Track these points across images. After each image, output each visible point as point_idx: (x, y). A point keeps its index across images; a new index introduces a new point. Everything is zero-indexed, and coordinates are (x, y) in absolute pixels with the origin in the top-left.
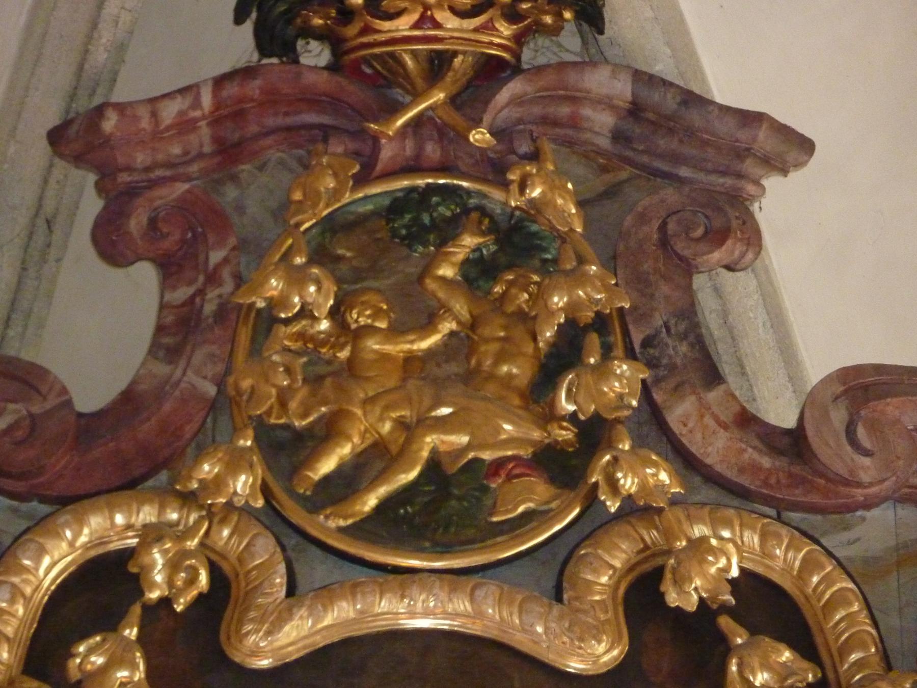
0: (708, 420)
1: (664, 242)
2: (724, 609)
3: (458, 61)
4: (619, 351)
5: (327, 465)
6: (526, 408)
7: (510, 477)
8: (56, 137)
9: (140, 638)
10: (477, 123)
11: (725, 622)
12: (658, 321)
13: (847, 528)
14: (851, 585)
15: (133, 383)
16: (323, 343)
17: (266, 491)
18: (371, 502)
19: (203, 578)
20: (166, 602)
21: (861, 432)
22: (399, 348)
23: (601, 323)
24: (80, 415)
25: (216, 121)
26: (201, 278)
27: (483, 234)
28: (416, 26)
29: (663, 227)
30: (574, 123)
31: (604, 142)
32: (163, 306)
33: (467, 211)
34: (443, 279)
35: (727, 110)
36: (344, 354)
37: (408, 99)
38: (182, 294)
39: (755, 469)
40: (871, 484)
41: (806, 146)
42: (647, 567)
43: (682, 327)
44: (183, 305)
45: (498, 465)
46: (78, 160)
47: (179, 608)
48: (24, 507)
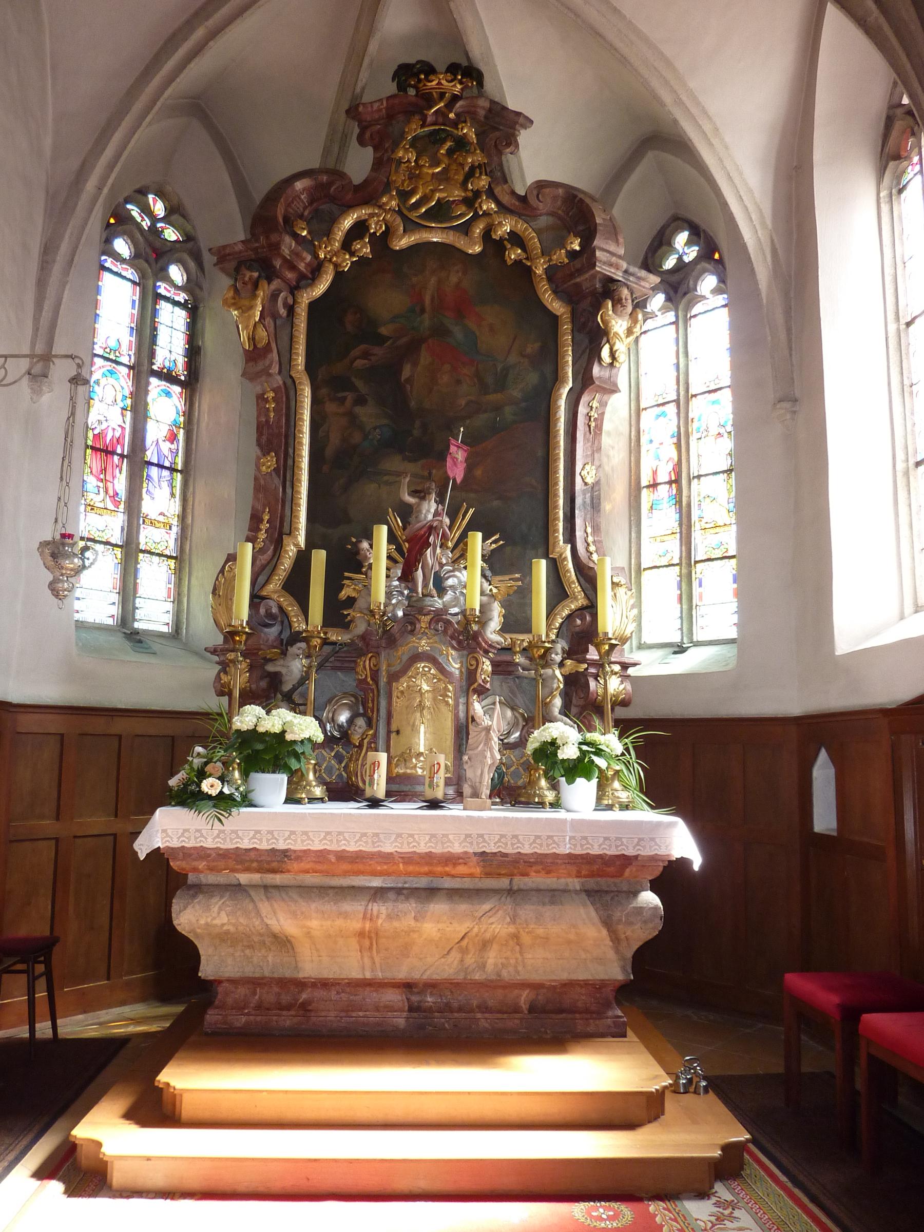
1: (496, 146)
2: (506, 239)
5: (413, 200)
7: (457, 205)
11: (506, 242)
18: (424, 210)
19: (384, 228)
20: (375, 233)
22: (430, 171)
23: (480, 166)
28: (437, 84)
29: (496, 142)
33: (448, 136)
36: (417, 172)
38: (378, 155)
41: (532, 122)
46: (353, 118)
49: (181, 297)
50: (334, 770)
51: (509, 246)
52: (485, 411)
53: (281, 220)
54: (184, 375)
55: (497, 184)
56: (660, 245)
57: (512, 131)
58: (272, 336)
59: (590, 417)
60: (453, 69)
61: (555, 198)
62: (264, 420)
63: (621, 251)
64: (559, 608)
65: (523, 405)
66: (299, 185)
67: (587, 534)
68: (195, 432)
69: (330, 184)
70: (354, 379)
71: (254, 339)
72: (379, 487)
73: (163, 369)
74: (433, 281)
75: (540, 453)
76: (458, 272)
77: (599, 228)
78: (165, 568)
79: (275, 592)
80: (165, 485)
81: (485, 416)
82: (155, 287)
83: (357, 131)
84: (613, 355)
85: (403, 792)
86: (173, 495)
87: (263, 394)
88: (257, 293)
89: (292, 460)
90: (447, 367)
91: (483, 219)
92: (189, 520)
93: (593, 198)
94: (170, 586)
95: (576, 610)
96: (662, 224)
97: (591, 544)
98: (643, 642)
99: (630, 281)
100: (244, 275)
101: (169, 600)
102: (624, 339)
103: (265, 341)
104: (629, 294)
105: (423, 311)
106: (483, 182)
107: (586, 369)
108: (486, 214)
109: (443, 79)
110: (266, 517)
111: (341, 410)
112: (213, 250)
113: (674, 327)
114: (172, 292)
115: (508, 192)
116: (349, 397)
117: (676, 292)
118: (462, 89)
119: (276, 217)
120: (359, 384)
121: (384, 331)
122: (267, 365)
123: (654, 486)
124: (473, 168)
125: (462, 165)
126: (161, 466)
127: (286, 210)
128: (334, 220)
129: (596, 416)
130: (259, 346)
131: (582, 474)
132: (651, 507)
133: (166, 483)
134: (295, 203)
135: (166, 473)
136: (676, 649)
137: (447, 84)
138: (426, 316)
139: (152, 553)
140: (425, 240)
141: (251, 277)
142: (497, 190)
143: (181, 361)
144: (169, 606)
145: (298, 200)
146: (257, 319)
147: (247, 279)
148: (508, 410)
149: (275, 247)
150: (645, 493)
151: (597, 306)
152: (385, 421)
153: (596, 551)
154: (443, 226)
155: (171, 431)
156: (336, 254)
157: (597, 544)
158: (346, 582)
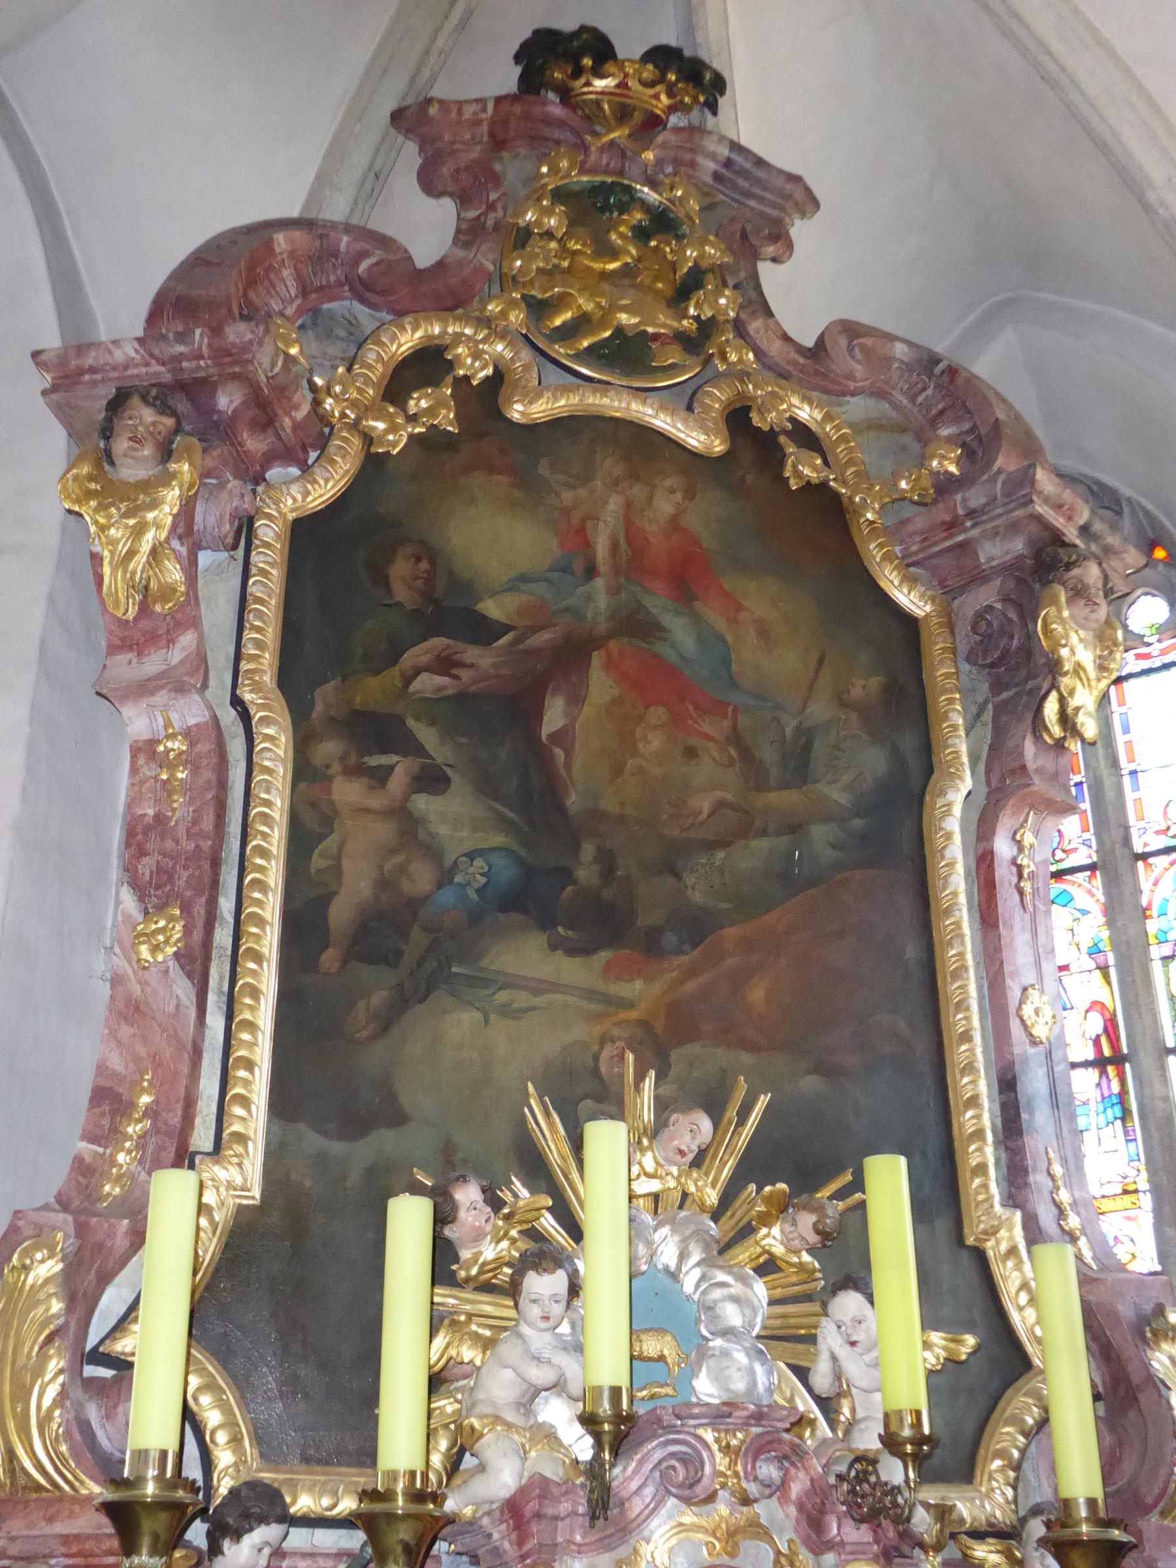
5: (558, 322)
7: (663, 344)
8: (397, 117)
9: (452, 395)
11: (782, 439)
13: (840, 405)
18: (585, 344)
20: (467, 378)
22: (597, 266)
25: (492, 123)
26: (484, 207)
29: (743, 229)
30: (692, 164)
35: (781, 172)
37: (603, 131)
38: (472, 214)
39: (795, 363)
40: (861, 380)
41: (816, 204)
42: (738, 405)
44: (473, 220)
45: (655, 337)
46: (408, 132)
47: (475, 383)
48: (378, 314)
52: (764, 832)
62: (151, 812)
65: (857, 823)
70: (411, 723)
72: (487, 1021)
74: (614, 503)
75: (912, 951)
76: (672, 491)
81: (762, 845)
90: (657, 714)
102: (1093, 683)
105: (591, 572)
109: (634, 76)
111: (376, 802)
112: (44, 357)
115: (779, 333)
116: (399, 769)
120: (427, 736)
121: (492, 608)
137: (640, 88)
138: (599, 583)
140: (594, 411)
142: (755, 326)
148: (821, 834)
152: (499, 839)
156: (366, 410)
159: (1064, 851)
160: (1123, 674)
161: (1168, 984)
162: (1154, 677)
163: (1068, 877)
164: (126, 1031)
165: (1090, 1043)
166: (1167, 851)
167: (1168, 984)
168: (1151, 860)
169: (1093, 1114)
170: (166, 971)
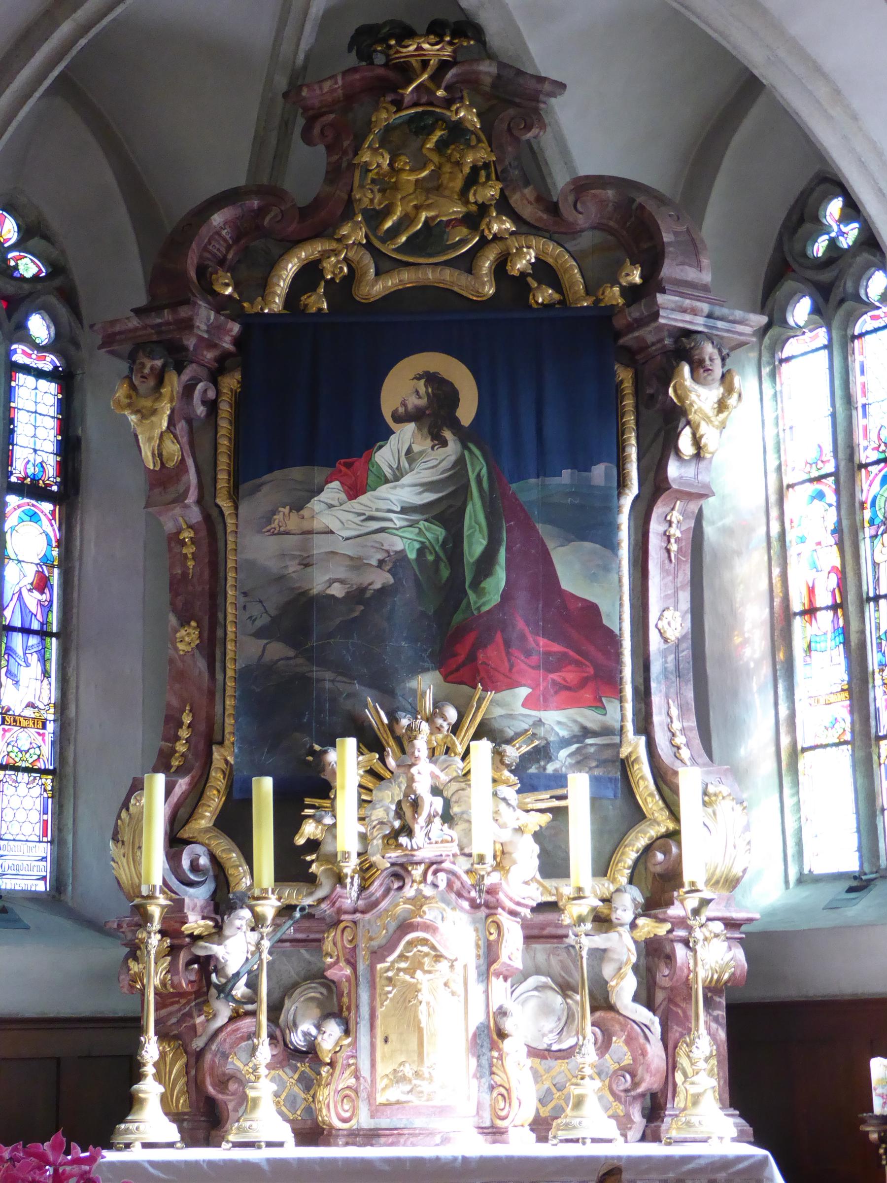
0: (525, 202)
1: (509, 130)
2: (529, 274)
3: (432, 62)
4: (493, 176)
5: (388, 224)
6: (460, 199)
7: (453, 227)
9: (325, 293)
10: (439, 88)
11: (529, 279)
12: (507, 163)
13: (574, 239)
14: (574, 263)
15: (318, 195)
16: (385, 176)
17: (367, 237)
19: (346, 270)
20: (332, 279)
21: (579, 206)
22: (413, 178)
23: (486, 166)
24: (299, 208)
27: (444, 130)
28: (416, 50)
29: (509, 125)
31: (488, 89)
32: (328, 163)
33: (437, 121)
34: (428, 148)
36: (393, 180)
38: (335, 158)
41: (562, 86)
43: (516, 163)
49: (48, 363)
50: (299, 1101)
51: (534, 284)
53: (193, 274)
54: (56, 483)
55: (514, 191)
56: (801, 221)
57: (534, 104)
58: (187, 448)
59: (669, 537)
60: (436, 29)
61: (602, 203)
62: (179, 572)
63: (706, 277)
64: (632, 836)
66: (217, 219)
67: (671, 718)
68: (77, 573)
69: (262, 212)
71: (160, 455)
73: (25, 479)
77: (670, 249)
78: (37, 791)
79: (207, 830)
80: (34, 659)
82: (9, 353)
83: (301, 122)
84: (696, 441)
85: (396, 1129)
86: (46, 674)
87: (179, 532)
88: (163, 391)
89: (222, 630)
91: (494, 245)
92: (72, 712)
93: (661, 199)
94: (45, 817)
95: (658, 838)
96: (801, 189)
97: (678, 733)
98: (806, 871)
99: (717, 328)
100: (143, 365)
101: (45, 839)
102: (713, 419)
103: (177, 458)
104: (716, 351)
106: (491, 192)
107: (661, 460)
108: (496, 238)
110: (187, 719)
113: (825, 353)
114: (34, 356)
117: (826, 300)
118: (454, 51)
119: (185, 272)
122: (181, 491)
123: (810, 612)
124: (475, 170)
125: (458, 164)
126: (26, 631)
127: (201, 257)
128: (272, 265)
129: (678, 534)
130: (170, 465)
131: (660, 626)
132: (809, 646)
133: (35, 656)
134: (213, 243)
135: (33, 640)
136: (855, 883)
139: (16, 769)
141: (152, 368)
142: (515, 200)
143: (51, 462)
144: (44, 849)
145: (217, 237)
146: (164, 428)
147: (147, 371)
149: (187, 325)
150: (798, 623)
151: (667, 375)
153: (687, 745)
154: (432, 260)
155: (40, 574)
157: (688, 733)
158: (308, 812)
159: (822, 462)
160: (864, 331)
161: (873, 555)
162: (880, 333)
163: (824, 480)
164: (177, 686)
165: (830, 594)
166: (878, 462)
167: (873, 555)
168: (870, 468)
169: (829, 641)
170: (193, 655)
